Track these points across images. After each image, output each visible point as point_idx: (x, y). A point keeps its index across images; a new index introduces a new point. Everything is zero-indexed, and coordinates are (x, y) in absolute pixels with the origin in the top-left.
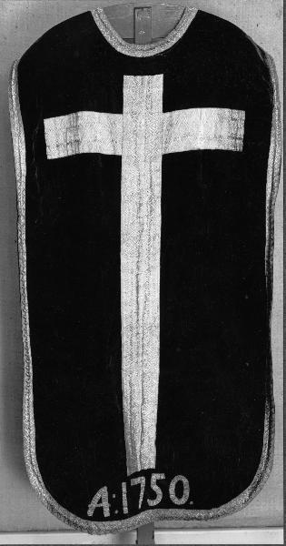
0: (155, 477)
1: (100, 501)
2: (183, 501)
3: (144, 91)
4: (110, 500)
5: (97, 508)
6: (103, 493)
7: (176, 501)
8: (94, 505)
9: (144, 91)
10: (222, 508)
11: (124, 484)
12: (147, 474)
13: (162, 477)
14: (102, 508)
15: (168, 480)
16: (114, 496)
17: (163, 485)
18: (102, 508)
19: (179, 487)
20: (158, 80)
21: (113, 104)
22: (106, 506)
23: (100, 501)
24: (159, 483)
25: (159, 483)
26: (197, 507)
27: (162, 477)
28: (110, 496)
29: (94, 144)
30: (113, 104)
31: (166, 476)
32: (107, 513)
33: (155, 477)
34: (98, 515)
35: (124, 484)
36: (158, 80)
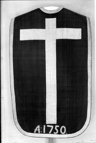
0: (56, 126)
1: (38, 129)
2: (64, 133)
3: (51, 22)
4: (40, 129)
5: (37, 131)
6: (38, 127)
7: (62, 133)
8: (36, 130)
9: (51, 22)
10: (17, 120)
11: (44, 126)
12: (54, 125)
13: (58, 126)
14: (38, 131)
15: (60, 127)
16: (41, 128)
17: (59, 129)
18: (38, 131)
19: (63, 129)
20: (55, 19)
21: (43, 26)
22: (39, 130)
23: (38, 129)
24: (57, 128)
25: (57, 128)
26: (68, 133)
27: (58, 126)
28: (40, 128)
29: (3, 100)
30: (43, 26)
31: (59, 126)
32: (39, 132)
33: (56, 126)
34: (37, 132)
35: (44, 126)
36: (55, 19)
